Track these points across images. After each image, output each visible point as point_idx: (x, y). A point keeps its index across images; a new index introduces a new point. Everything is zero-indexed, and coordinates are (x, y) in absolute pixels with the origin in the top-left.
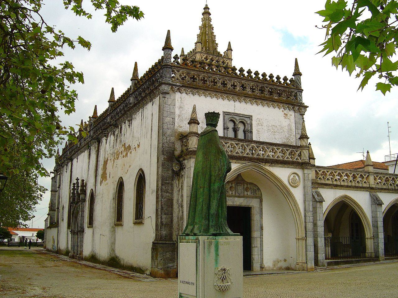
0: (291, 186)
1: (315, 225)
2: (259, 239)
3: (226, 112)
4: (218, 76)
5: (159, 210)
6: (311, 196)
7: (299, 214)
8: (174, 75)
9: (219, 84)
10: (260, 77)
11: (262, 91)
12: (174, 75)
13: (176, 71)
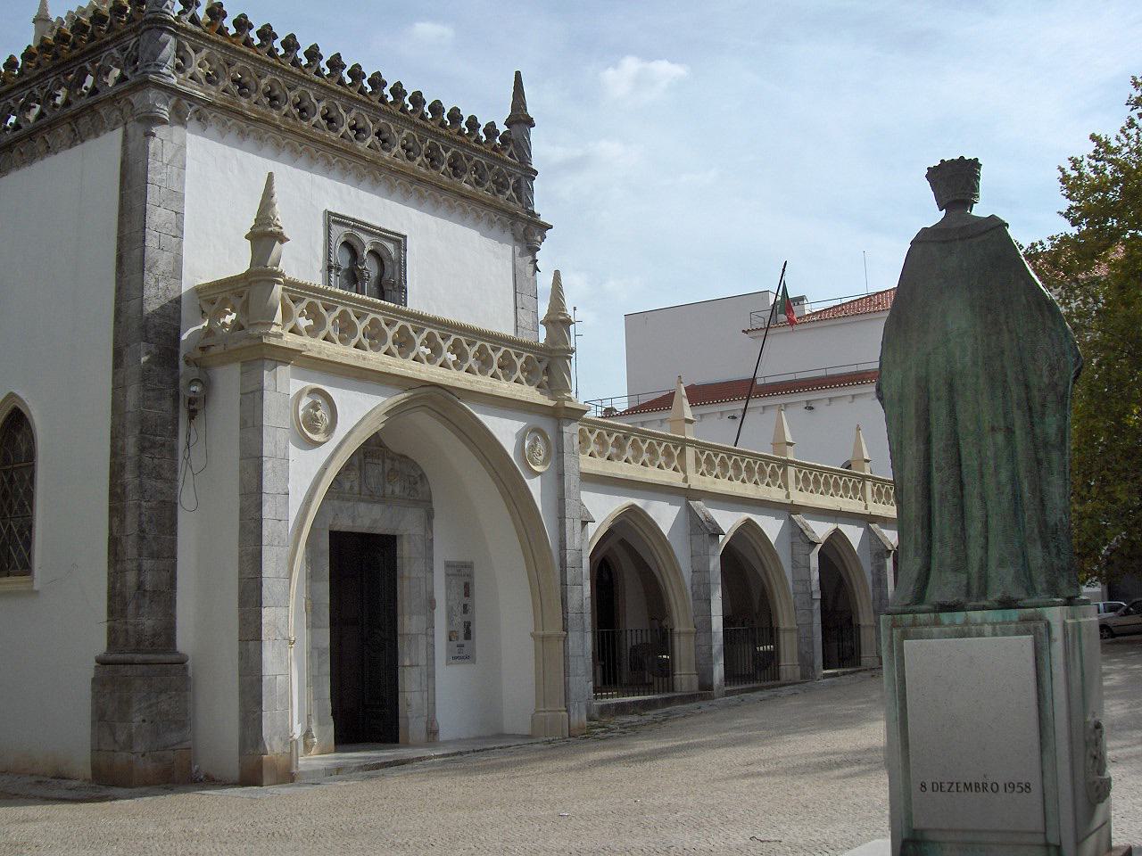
3: (336, 215)
4: (313, 89)
10: (228, 29)
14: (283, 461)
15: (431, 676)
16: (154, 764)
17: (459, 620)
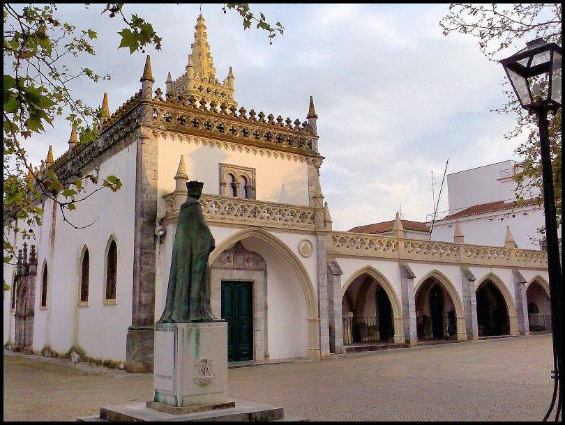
0: (301, 254)
1: (331, 302)
2: (263, 322)
5: (138, 286)
6: (326, 268)
7: (311, 291)
8: (156, 115)
9: (215, 129)
11: (268, 137)
12: (156, 115)
13: (158, 110)
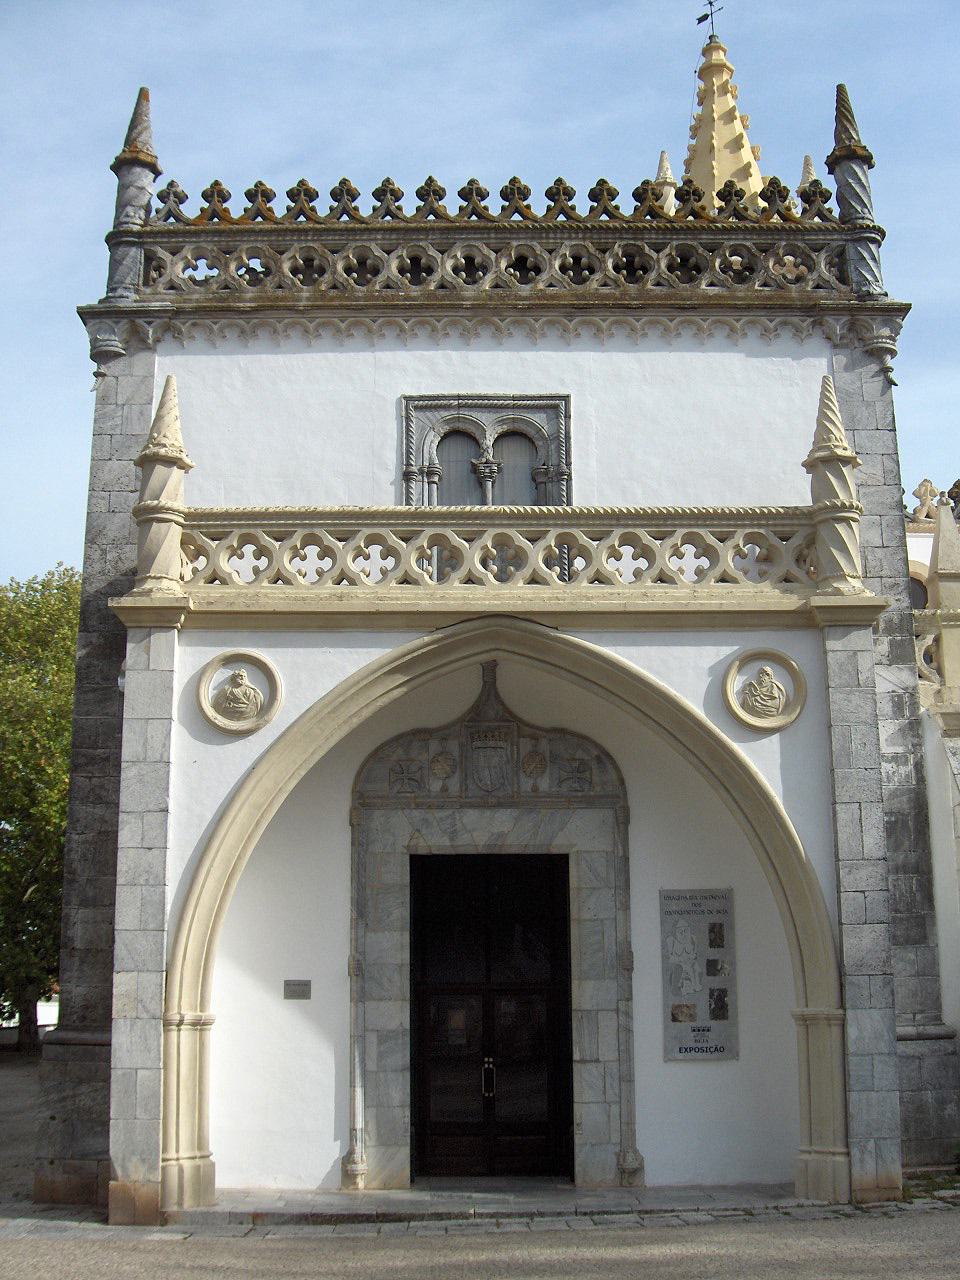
3: (421, 398)
14: (160, 765)
15: (627, 1079)
16: (66, 1176)
17: (696, 991)
